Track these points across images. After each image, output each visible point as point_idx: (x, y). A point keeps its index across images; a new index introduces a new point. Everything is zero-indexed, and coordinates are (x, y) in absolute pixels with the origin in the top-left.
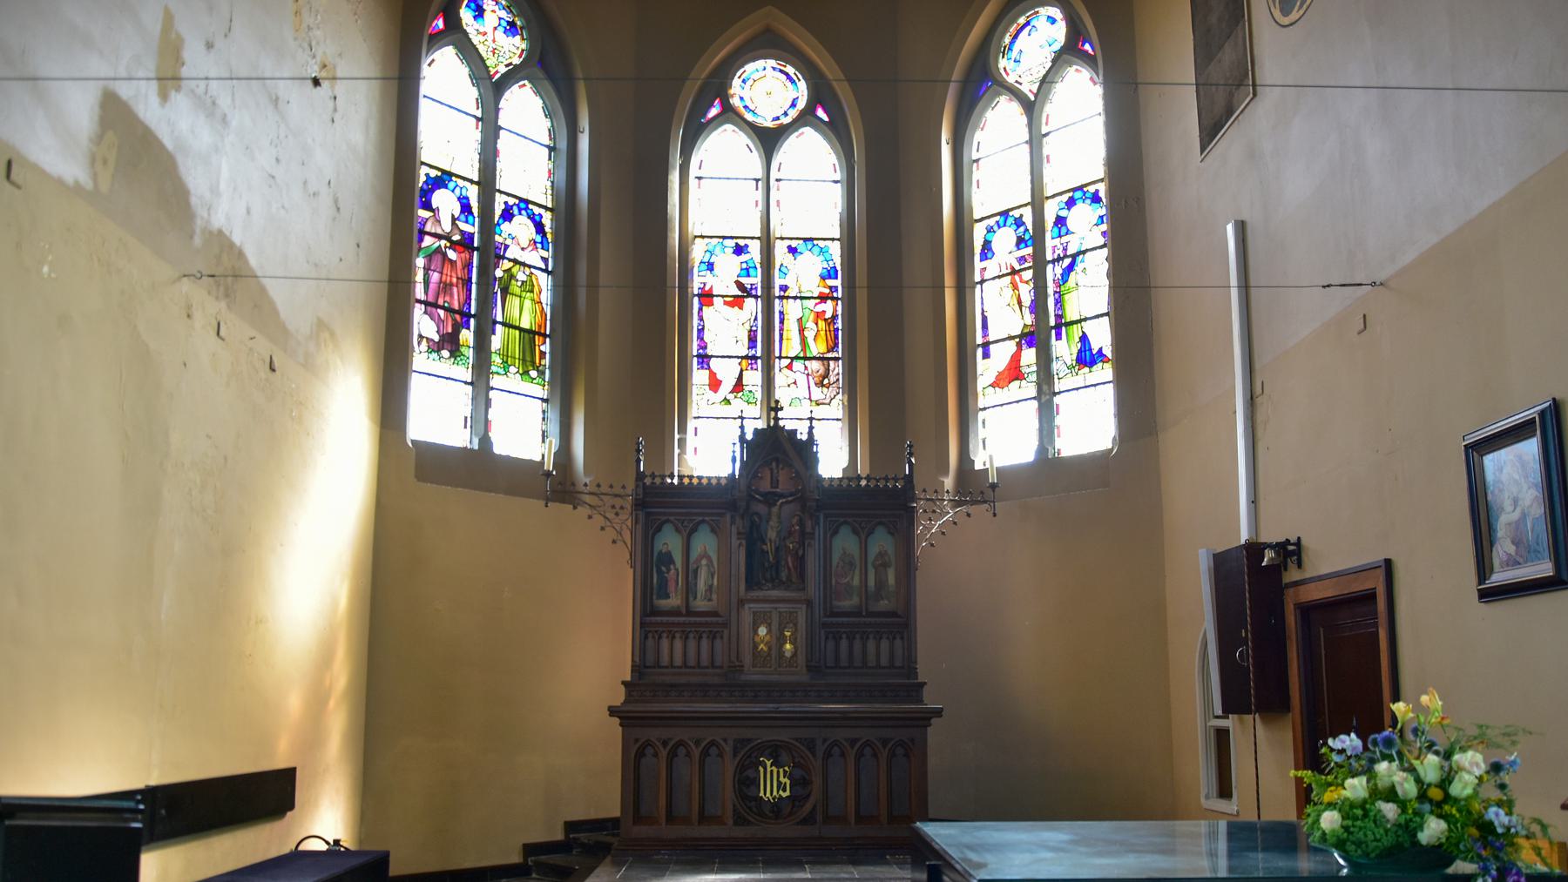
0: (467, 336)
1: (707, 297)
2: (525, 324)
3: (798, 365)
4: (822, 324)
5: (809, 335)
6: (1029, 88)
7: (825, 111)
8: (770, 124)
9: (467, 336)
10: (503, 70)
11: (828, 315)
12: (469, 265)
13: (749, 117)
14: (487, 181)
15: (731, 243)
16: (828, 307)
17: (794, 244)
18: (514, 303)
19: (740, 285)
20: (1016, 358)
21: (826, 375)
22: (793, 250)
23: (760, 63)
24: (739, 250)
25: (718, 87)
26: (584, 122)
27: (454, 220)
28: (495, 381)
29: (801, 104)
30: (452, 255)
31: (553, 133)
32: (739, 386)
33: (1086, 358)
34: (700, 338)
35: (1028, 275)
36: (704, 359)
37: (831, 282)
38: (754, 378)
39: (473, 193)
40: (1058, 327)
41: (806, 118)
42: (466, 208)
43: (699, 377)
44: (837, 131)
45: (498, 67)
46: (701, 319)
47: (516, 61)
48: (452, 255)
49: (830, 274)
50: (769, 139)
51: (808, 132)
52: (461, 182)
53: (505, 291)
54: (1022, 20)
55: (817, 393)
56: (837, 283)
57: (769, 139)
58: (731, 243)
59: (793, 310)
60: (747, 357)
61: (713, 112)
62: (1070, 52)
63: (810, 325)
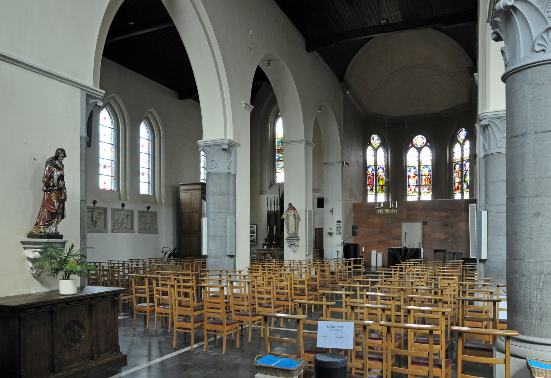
0: (374, 188)
1: (409, 176)
2: (382, 185)
3: (424, 186)
4: (428, 180)
5: (426, 181)
6: (461, 142)
7: (429, 143)
8: (419, 147)
9: (374, 188)
10: (377, 147)
11: (430, 178)
12: (373, 178)
13: (416, 146)
14: (376, 165)
15: (413, 167)
16: (429, 177)
17: (424, 167)
18: (380, 182)
19: (415, 174)
20: (458, 186)
21: (429, 188)
22: (423, 168)
23: (418, 136)
24: (415, 168)
25: (411, 142)
26: (389, 152)
27: (371, 172)
28: (378, 194)
29: (425, 143)
30: (371, 177)
31: (385, 155)
32: (415, 190)
33: (468, 187)
34: (408, 183)
35: (460, 173)
36: (409, 186)
37: (430, 173)
38: (417, 189)
39: (374, 167)
40: (464, 182)
41: (426, 145)
42: (373, 170)
43: (408, 189)
44: (430, 147)
45: (376, 147)
46: (409, 180)
47: (379, 145)
48: (371, 177)
49: (430, 171)
50: (419, 150)
51: (426, 147)
52: (372, 166)
53: (379, 180)
54: (461, 130)
55: (428, 191)
56: (431, 172)
57: (419, 150)
58: (413, 167)
59: (424, 177)
60: (416, 186)
61: (410, 145)
62: (467, 138)
63: (426, 180)
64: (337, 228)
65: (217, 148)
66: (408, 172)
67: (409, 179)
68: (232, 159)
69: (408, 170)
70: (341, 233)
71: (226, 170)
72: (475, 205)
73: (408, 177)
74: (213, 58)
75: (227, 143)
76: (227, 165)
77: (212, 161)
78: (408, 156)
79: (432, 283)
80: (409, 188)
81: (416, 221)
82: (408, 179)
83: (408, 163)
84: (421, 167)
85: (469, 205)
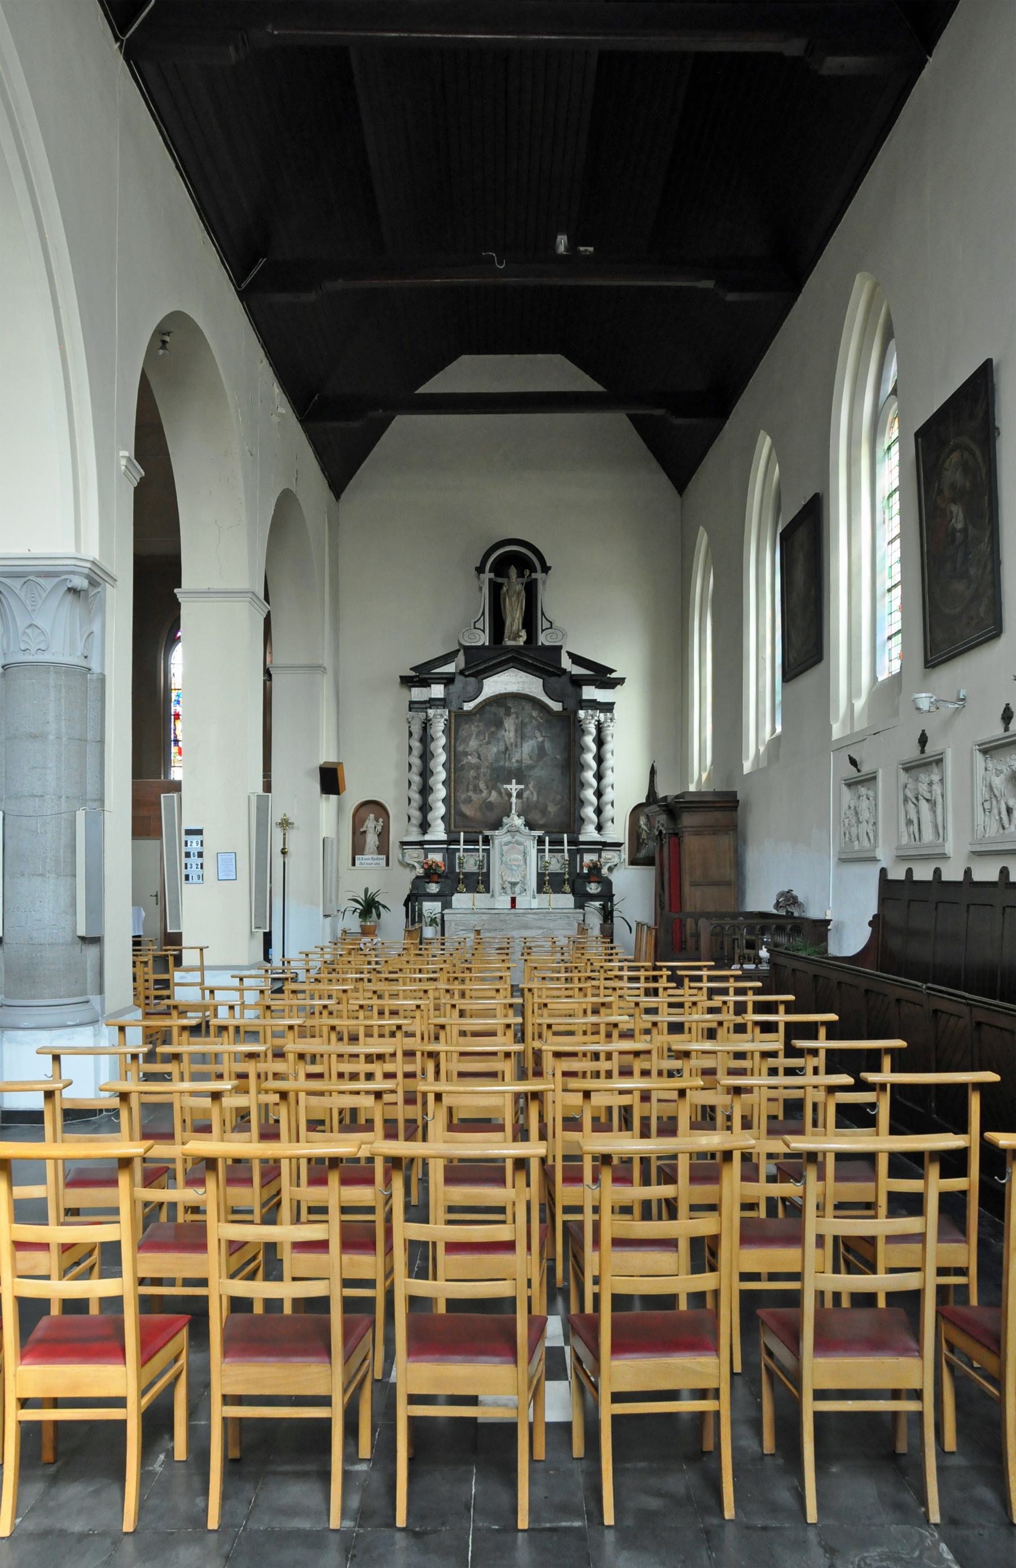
34: (175, 733)
36: (176, 742)
43: (174, 750)
46: (175, 725)
64: (200, 855)
65: (48, 583)
66: (172, 704)
67: (176, 724)
68: (96, 627)
69: (174, 697)
70: (186, 868)
71: (76, 660)
72: (175, 795)
73: (173, 717)
74: (48, 273)
75: (86, 571)
76: (80, 645)
77: (30, 625)
78: (172, 661)
79: (398, 990)
80: (177, 748)
81: (149, 835)
82: (175, 721)
83: (173, 679)
84: (173, 691)
85: (162, 795)
